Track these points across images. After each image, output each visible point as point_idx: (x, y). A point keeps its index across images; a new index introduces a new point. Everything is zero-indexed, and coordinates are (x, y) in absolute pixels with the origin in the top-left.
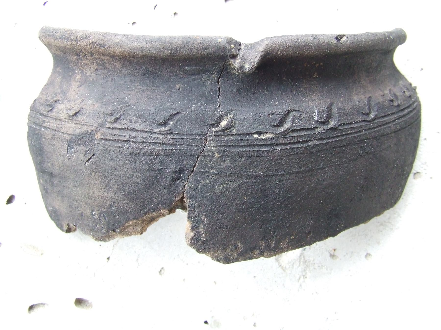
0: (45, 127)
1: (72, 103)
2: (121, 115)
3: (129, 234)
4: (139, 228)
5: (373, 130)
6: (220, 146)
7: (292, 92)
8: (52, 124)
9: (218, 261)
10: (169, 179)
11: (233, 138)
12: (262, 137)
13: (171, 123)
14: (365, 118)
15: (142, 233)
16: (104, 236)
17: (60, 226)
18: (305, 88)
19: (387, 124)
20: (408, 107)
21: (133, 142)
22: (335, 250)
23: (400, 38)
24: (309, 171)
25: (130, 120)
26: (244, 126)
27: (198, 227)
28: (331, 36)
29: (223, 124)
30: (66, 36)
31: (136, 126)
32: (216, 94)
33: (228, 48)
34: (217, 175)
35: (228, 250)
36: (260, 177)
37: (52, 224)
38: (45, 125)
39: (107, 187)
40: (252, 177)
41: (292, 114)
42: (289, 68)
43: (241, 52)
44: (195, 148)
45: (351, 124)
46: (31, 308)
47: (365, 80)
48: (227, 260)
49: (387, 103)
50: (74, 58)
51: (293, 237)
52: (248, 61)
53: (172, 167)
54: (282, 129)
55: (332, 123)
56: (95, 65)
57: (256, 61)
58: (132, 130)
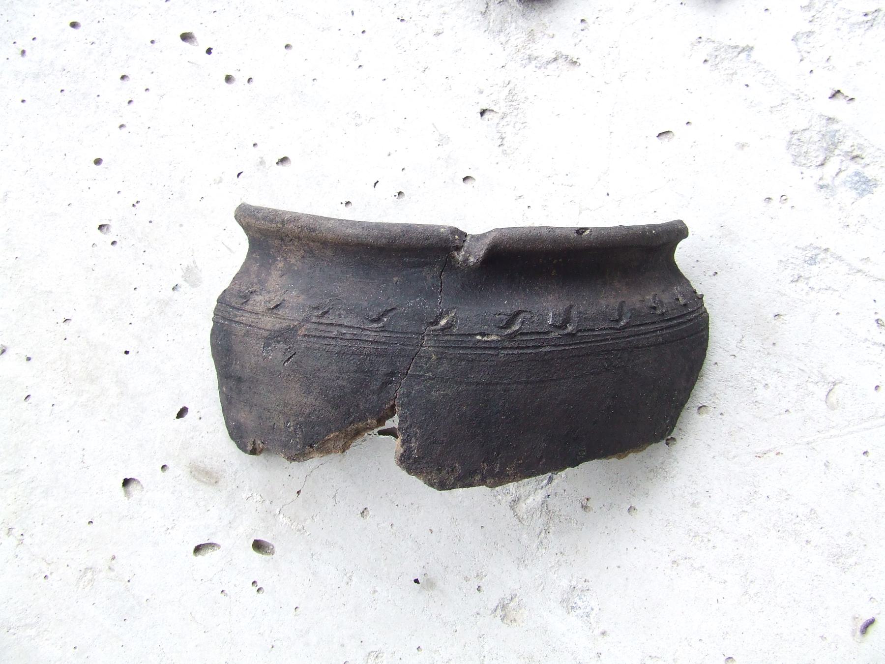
0: (237, 322)
1: (272, 295)
2: (329, 309)
3: (328, 452)
4: (341, 444)
5: (622, 340)
6: (438, 347)
7: (524, 290)
8: (246, 318)
9: (432, 485)
10: (379, 383)
11: (453, 338)
12: (486, 338)
14: (612, 325)
15: (343, 451)
16: (298, 455)
17: (242, 447)
18: (540, 288)
19: (642, 334)
20: (679, 317)
21: (341, 339)
22: (588, 499)
23: (676, 232)
24: (541, 381)
27: (409, 442)
28: (571, 229)
29: (443, 322)
30: (272, 216)
31: (345, 322)
34: (434, 379)
35: (444, 472)
36: (483, 384)
37: (232, 446)
38: (237, 319)
39: (308, 392)
40: (472, 383)
42: (526, 261)
43: (466, 244)
44: (410, 348)
45: (593, 330)
46: (198, 549)
47: (619, 282)
48: (442, 486)
49: (646, 310)
50: (277, 242)
51: (521, 462)
52: (473, 255)
53: (383, 369)
54: (509, 331)
55: (570, 328)
56: (302, 252)
57: (482, 253)
58: (340, 325)
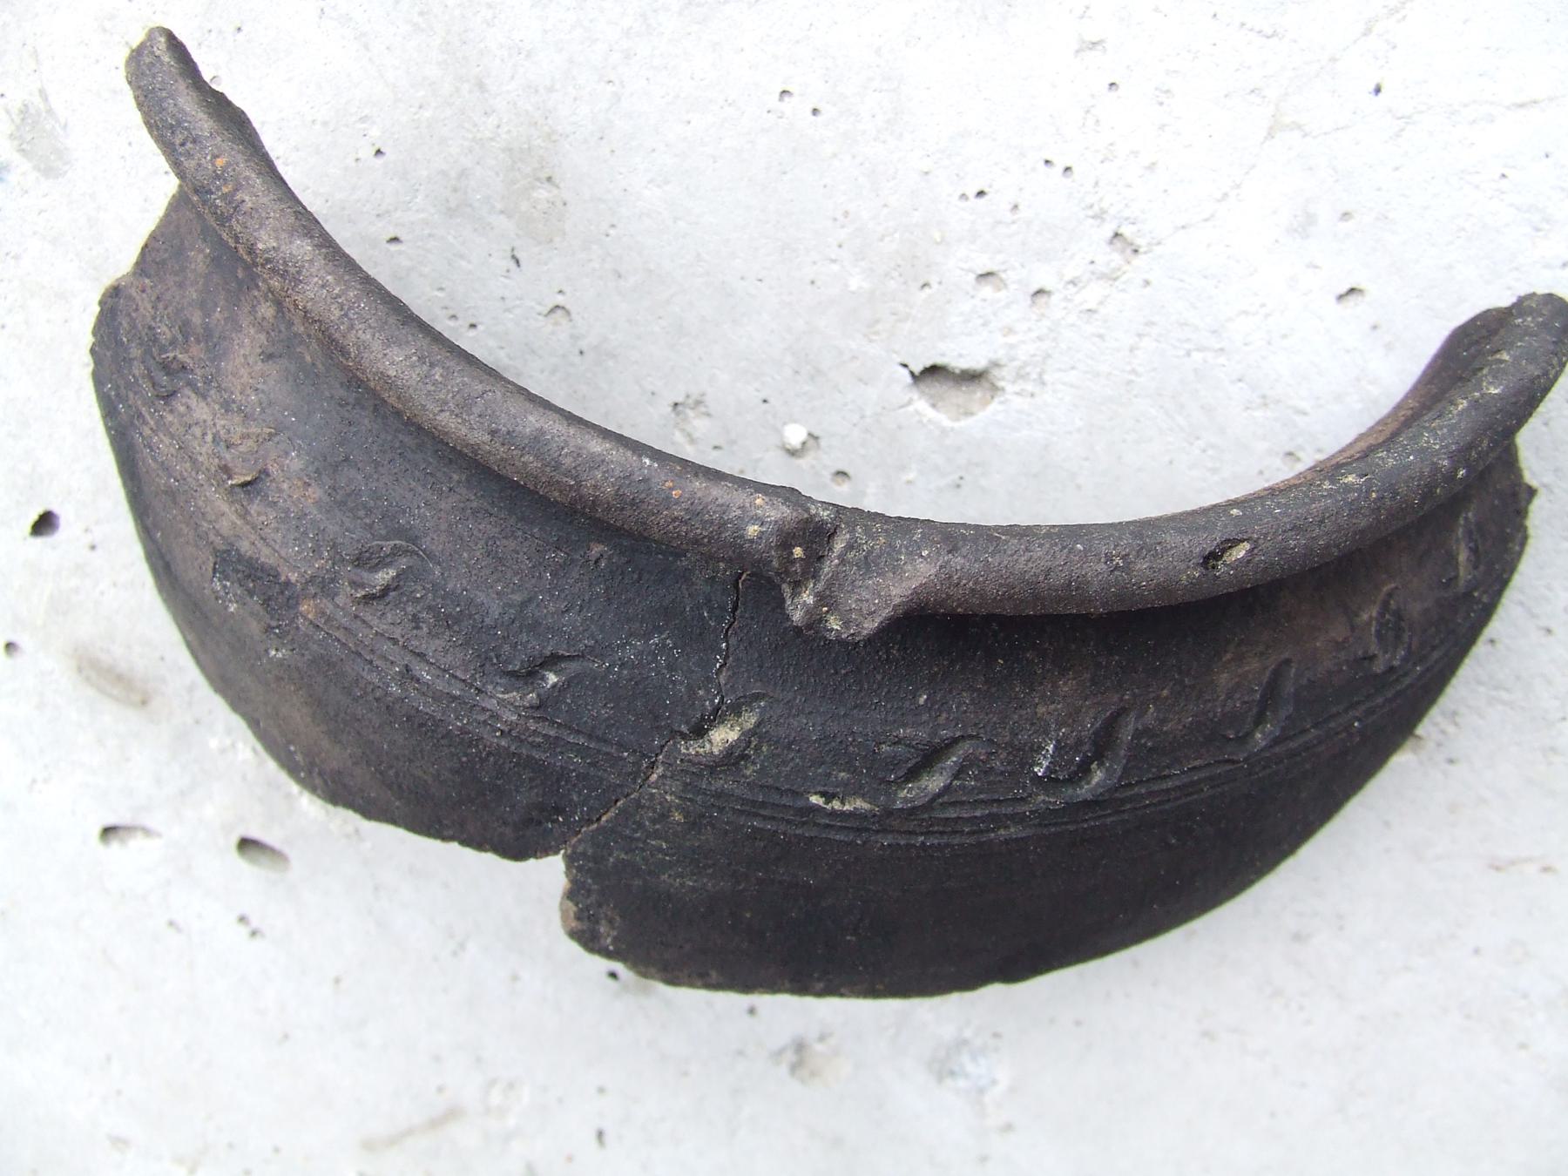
13: (552, 678)
25: (414, 615)
26: (784, 763)
32: (720, 620)
33: (775, 564)
41: (964, 748)
46: (108, 832)
